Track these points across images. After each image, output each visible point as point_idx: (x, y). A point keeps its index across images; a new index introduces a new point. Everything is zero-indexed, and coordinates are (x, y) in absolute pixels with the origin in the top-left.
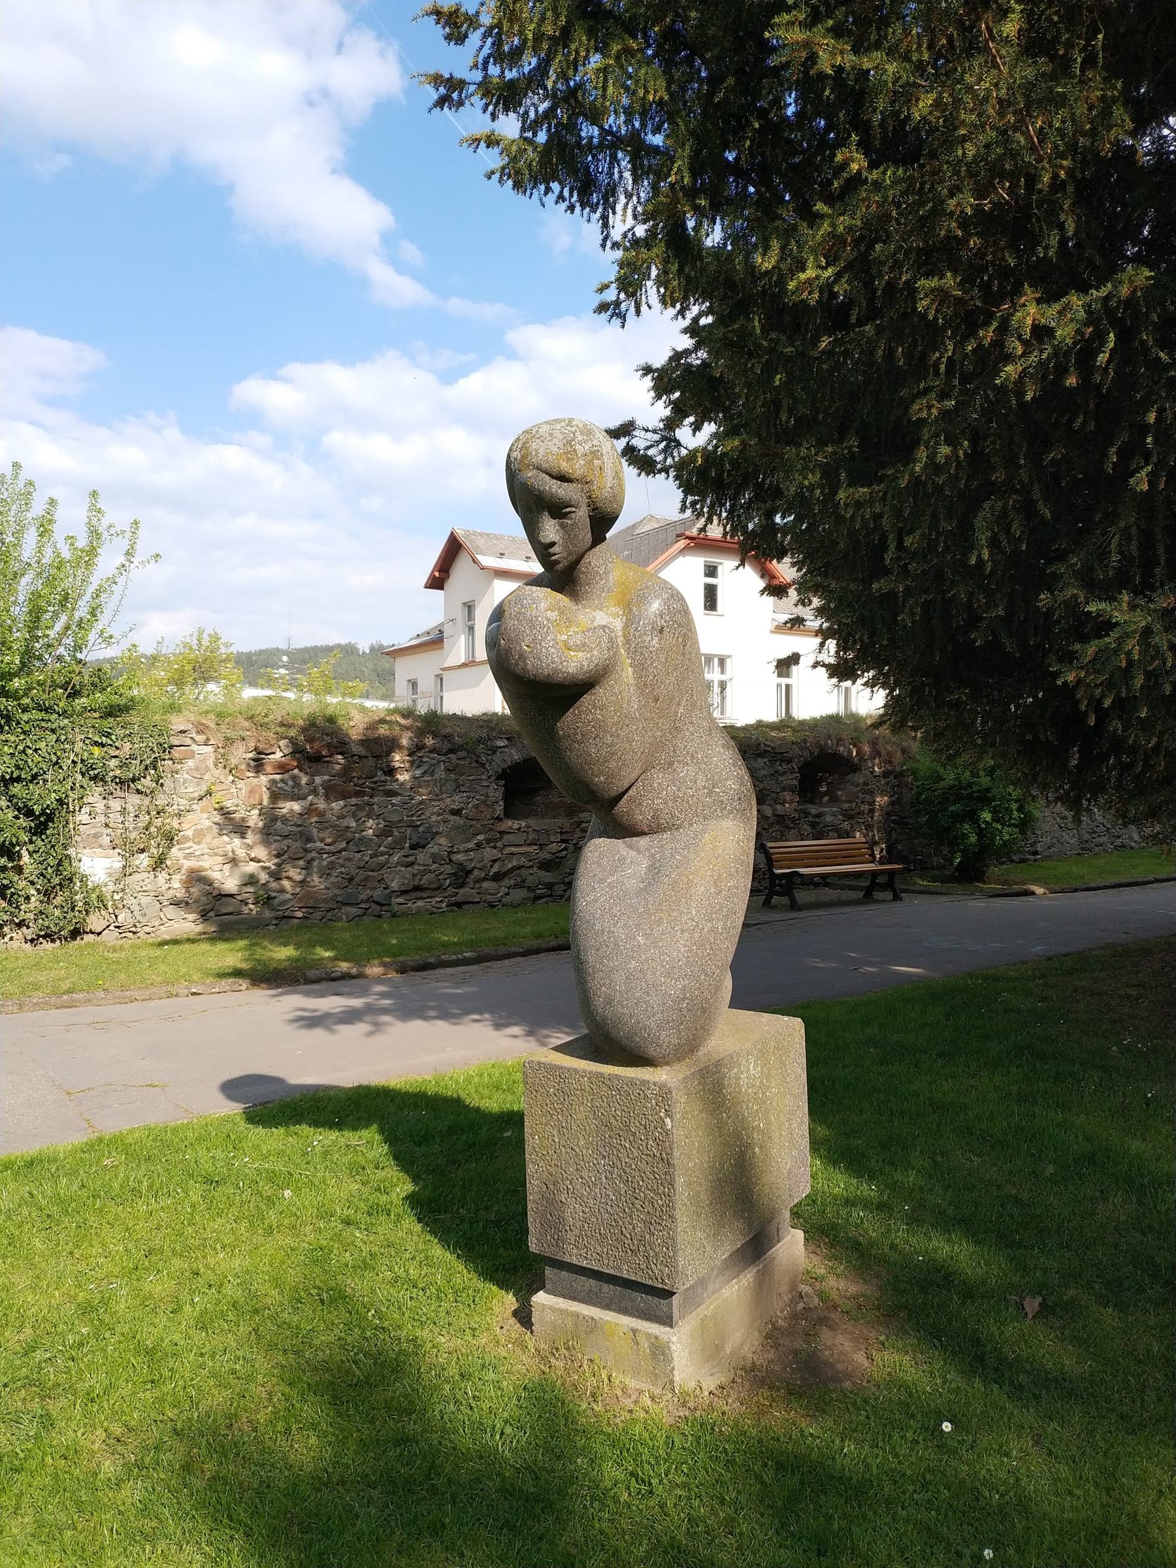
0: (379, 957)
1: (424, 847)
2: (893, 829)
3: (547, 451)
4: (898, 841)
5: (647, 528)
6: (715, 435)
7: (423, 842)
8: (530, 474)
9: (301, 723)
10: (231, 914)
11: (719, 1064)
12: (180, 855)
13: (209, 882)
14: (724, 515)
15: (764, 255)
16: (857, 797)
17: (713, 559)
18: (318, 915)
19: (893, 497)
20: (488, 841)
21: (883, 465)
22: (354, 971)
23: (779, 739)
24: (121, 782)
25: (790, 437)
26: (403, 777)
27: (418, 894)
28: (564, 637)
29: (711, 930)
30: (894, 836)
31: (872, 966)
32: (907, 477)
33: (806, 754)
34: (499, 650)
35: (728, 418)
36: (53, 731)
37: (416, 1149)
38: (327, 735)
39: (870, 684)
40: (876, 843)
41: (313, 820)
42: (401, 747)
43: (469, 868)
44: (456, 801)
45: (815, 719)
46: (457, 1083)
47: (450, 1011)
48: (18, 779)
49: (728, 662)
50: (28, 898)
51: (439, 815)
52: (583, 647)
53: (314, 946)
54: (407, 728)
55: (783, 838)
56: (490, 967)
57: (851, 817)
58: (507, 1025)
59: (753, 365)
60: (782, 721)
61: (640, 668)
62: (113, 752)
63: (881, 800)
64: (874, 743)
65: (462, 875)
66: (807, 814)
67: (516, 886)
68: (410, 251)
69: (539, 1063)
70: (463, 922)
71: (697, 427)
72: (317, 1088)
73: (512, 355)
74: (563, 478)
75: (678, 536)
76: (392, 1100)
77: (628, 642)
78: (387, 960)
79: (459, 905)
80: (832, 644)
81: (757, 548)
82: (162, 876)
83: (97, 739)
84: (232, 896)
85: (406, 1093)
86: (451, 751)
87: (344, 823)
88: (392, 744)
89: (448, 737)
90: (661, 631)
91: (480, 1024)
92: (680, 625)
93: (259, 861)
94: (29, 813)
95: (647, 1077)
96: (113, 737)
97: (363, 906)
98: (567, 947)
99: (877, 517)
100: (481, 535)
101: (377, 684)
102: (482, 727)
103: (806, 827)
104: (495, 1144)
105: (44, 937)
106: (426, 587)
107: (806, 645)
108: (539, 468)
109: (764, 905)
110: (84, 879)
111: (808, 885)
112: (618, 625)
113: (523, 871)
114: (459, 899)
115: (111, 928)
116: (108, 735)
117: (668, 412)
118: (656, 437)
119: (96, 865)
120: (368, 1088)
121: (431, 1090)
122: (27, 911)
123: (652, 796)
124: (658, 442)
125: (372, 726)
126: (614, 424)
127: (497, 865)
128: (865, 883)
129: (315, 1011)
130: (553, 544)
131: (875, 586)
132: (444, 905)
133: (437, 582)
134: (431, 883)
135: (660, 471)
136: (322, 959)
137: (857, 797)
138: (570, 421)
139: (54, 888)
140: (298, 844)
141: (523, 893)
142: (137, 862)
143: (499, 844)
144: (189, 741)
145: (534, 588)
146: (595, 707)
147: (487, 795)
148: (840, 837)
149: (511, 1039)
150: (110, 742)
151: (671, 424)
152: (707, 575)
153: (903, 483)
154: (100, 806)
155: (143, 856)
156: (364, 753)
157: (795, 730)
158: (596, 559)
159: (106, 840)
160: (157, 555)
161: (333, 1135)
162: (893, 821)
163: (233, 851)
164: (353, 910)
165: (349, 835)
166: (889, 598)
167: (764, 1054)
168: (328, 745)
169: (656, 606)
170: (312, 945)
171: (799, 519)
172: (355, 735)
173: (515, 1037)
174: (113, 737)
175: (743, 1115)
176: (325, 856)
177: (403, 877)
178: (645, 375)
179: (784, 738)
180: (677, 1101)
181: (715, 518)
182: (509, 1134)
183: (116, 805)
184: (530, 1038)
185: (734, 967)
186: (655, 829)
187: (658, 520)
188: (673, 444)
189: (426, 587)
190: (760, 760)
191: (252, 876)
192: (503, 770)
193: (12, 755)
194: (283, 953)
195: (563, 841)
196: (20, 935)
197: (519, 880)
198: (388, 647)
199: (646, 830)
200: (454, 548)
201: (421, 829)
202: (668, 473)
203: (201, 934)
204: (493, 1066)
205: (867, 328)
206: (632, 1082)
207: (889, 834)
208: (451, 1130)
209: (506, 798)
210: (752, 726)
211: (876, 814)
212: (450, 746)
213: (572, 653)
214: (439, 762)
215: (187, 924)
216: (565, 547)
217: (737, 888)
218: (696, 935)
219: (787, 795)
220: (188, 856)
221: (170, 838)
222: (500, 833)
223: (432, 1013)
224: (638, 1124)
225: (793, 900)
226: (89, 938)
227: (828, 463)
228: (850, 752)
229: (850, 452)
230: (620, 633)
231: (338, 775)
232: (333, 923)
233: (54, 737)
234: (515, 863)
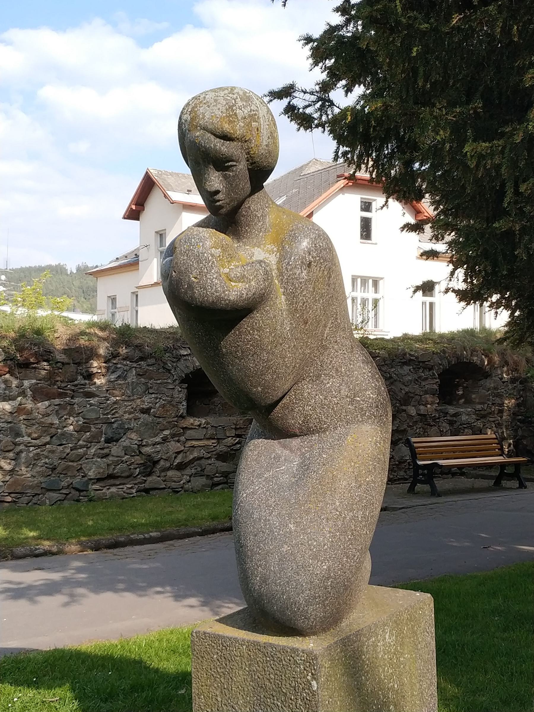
0: (77, 536)
1: (117, 441)
2: (519, 427)
3: (212, 115)
4: (523, 437)
5: (312, 169)
6: (363, 97)
7: (118, 436)
8: (198, 134)
9: (12, 334)
11: (358, 633)
14: (371, 163)
16: (489, 400)
17: (368, 196)
18: (25, 499)
19: (511, 151)
20: (173, 436)
21: (506, 123)
22: (55, 549)
23: (422, 349)
25: (425, 99)
26: (99, 381)
27: (112, 481)
28: (227, 270)
29: (354, 518)
30: (520, 433)
31: (499, 545)
32: (521, 134)
33: (445, 362)
34: (171, 281)
35: (376, 80)
37: (102, 705)
38: (35, 345)
39: (496, 305)
40: (503, 439)
41: (22, 418)
42: (98, 356)
43: (156, 459)
44: (146, 401)
45: (452, 333)
46: (140, 647)
47: (138, 584)
49: (381, 283)
51: (130, 413)
52: (242, 279)
53: (21, 527)
54: (104, 339)
56: (172, 545)
57: (484, 417)
58: (186, 596)
59: (394, 39)
60: (424, 334)
61: (291, 296)
63: (509, 403)
64: (502, 354)
65: (150, 465)
67: (196, 475)
69: (205, 633)
70: (150, 505)
71: (348, 89)
72: (20, 651)
73: (199, 24)
74: (225, 137)
75: (338, 176)
76: (83, 662)
77: (281, 274)
78: (83, 539)
79: (147, 491)
80: (460, 273)
81: (403, 190)
85: (96, 656)
86: (142, 359)
87: (49, 420)
88: (91, 353)
89: (139, 347)
90: (309, 265)
91: (162, 596)
92: (325, 260)
95: (297, 646)
97: (64, 491)
98: (230, 529)
99: (498, 167)
100: (171, 174)
101: (83, 299)
102: (169, 338)
103: (444, 424)
104: (171, 701)
106: (124, 218)
107: (439, 271)
108: (205, 129)
111: (447, 474)
112: (273, 260)
113: (203, 461)
114: (147, 485)
117: (324, 76)
118: (313, 98)
120: (62, 651)
121: (117, 653)
123: (307, 401)
124: (315, 102)
125: (74, 338)
126: (277, 86)
127: (180, 456)
128: (495, 473)
129: (20, 583)
130: (217, 192)
131: (496, 225)
132: (134, 491)
133: (134, 214)
134: (122, 472)
135: (317, 126)
136: (27, 538)
137: (489, 400)
138: (233, 89)
140: (9, 439)
141: (203, 481)
143: (182, 438)
145: (201, 229)
146: (253, 329)
147: (172, 397)
149: (187, 608)
151: (326, 87)
152: (363, 209)
153: (518, 139)
156: (66, 360)
157: (435, 343)
158: (254, 204)
161: (31, 693)
162: (519, 421)
164: (55, 495)
165: (53, 430)
166: (509, 234)
167: (398, 625)
168: (36, 354)
169: (305, 244)
170: (19, 526)
171: (434, 167)
172: (59, 345)
173: (192, 607)
175: (380, 678)
176: (31, 449)
177: (99, 467)
178: (307, 44)
179: (426, 350)
180: (322, 666)
181: (363, 166)
182: (183, 692)
184: (205, 608)
185: (372, 549)
186: (305, 431)
187: (321, 163)
188: (327, 103)
189: (124, 218)
190: (406, 368)
192: (187, 375)
195: (238, 436)
197: (199, 469)
198: (93, 268)
199: (297, 432)
200: (148, 186)
201: (115, 426)
202: (324, 127)
204: (172, 632)
205: (491, 8)
206: (284, 650)
207: (516, 431)
208: (134, 688)
209: (189, 399)
210: (399, 338)
211: (505, 414)
212: (141, 355)
213: (233, 284)
214: (131, 368)
216: (228, 194)
217: (374, 482)
218: (340, 523)
219: (429, 398)
222: (183, 428)
223: (121, 586)
224: (288, 686)
225: (433, 487)
227: (457, 121)
228: (482, 361)
229: (475, 112)
230: (275, 267)
231: (44, 379)
232: (37, 506)
234: (195, 454)
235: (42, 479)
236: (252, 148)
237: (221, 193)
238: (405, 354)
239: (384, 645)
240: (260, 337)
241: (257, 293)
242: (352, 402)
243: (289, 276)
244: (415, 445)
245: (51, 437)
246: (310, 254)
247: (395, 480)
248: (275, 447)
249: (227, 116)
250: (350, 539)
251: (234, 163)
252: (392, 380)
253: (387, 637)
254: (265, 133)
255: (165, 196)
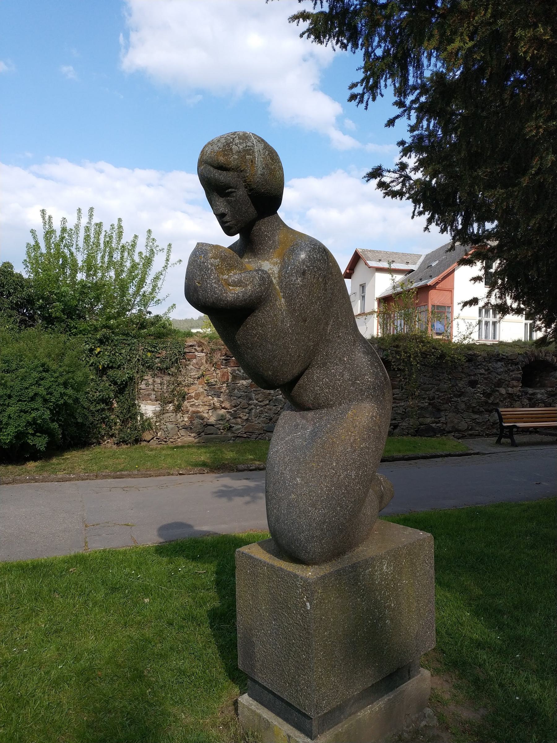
10: (212, 434)
12: (188, 405)
13: (202, 418)
15: (429, 40)
18: (254, 436)
24: (160, 369)
28: (226, 277)
29: (346, 476)
33: (526, 360)
36: (129, 345)
48: (112, 368)
50: (116, 424)
55: (511, 406)
61: (290, 299)
62: (157, 356)
66: (526, 393)
68: (349, 124)
82: (179, 415)
83: (149, 349)
84: (213, 425)
90: (304, 273)
93: (226, 409)
94: (115, 383)
96: (158, 348)
100: (370, 251)
103: (525, 400)
105: (123, 442)
109: (496, 443)
110: (142, 415)
111: (526, 432)
115: (155, 439)
116: (155, 347)
118: (397, 175)
119: (148, 409)
122: (115, 430)
129: (230, 487)
139: (127, 419)
142: (168, 408)
144: (193, 351)
146: (257, 325)
148: (546, 406)
150: (156, 350)
154: (151, 381)
155: (170, 405)
159: (153, 397)
160: (180, 261)
163: (214, 404)
174: (158, 348)
176: (258, 407)
183: (158, 380)
186: (315, 407)
190: (499, 363)
191: (222, 416)
193: (109, 356)
194: (229, 455)
196: (112, 441)
203: (196, 443)
213: (231, 288)
215: (189, 438)
217: (368, 448)
219: (515, 383)
220: (192, 406)
221: (184, 397)
226: (143, 444)
233: (129, 348)
235: (264, 425)
236: (247, 176)
237: (227, 216)
238: (499, 355)
239: (380, 574)
240: (263, 332)
241: (254, 296)
242: (353, 384)
243: (287, 282)
244: (502, 413)
245: (270, 401)
246: (304, 264)
247: (490, 435)
248: (297, 417)
249: (222, 151)
250: (343, 493)
251: (233, 190)
252: (489, 371)
253: (385, 568)
254: (260, 164)
255: (366, 264)
